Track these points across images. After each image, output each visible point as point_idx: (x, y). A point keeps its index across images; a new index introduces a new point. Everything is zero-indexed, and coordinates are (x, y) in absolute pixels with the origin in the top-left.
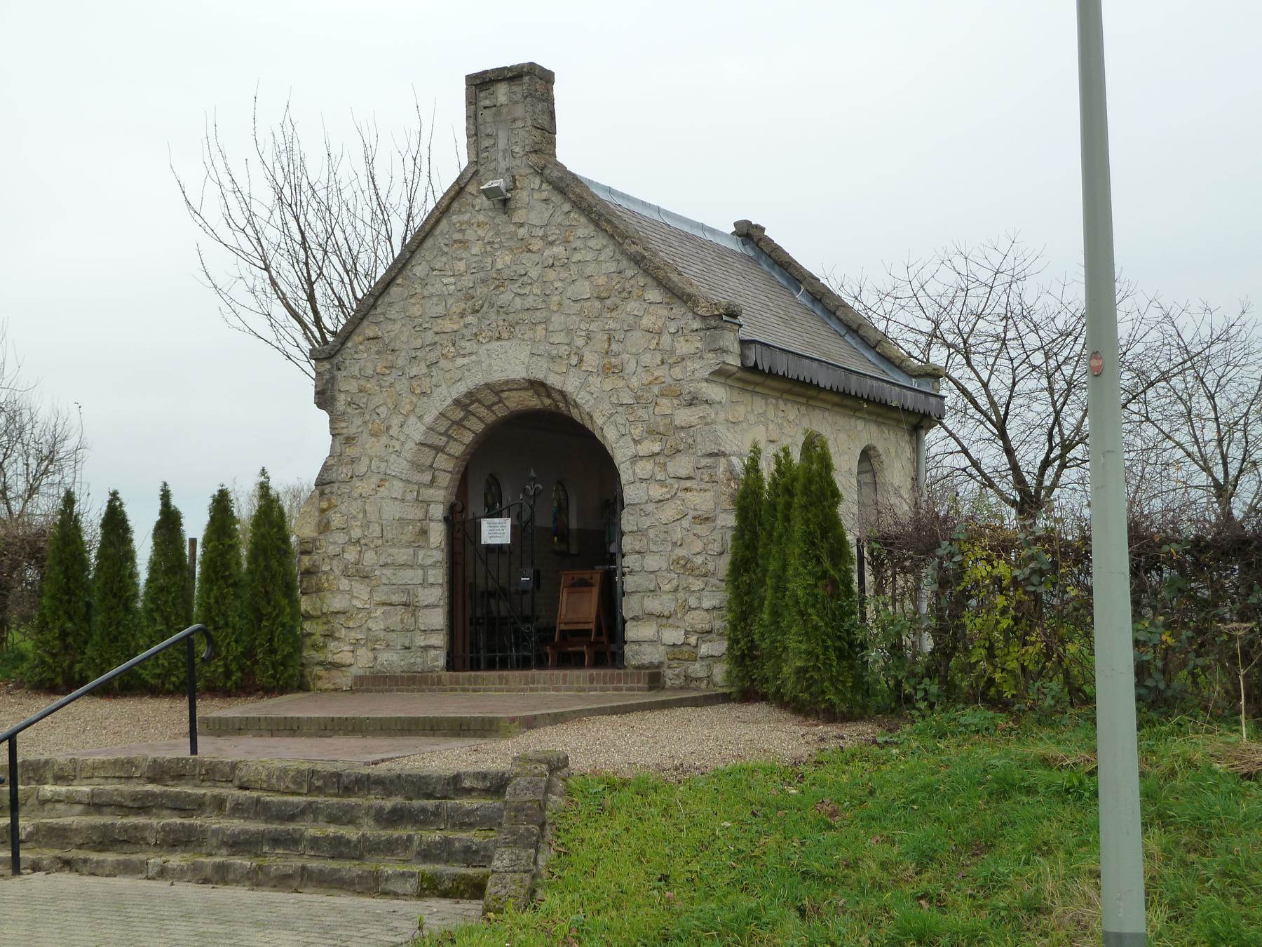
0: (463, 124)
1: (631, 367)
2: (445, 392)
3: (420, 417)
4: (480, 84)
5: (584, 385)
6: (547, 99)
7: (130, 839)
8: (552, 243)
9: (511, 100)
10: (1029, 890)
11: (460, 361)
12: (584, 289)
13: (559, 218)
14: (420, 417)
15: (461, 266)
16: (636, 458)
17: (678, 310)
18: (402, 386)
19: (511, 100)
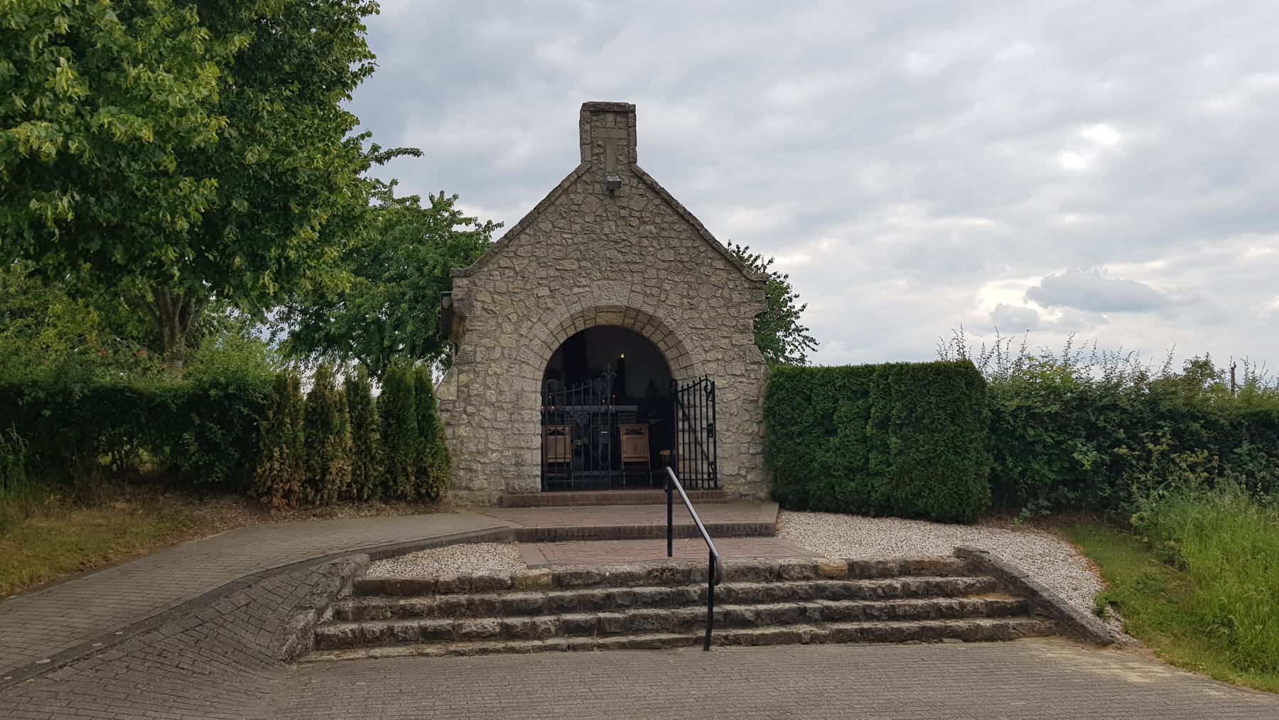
0: (662, 184)
1: (703, 306)
2: (565, 309)
3: (546, 324)
4: (593, 112)
5: (670, 314)
6: (631, 127)
7: (531, 632)
8: (646, 223)
9: (608, 124)
10: (162, 525)
11: (576, 290)
12: (669, 255)
13: (651, 207)
14: (546, 324)
15: (577, 228)
16: (706, 361)
17: (736, 275)
18: (531, 302)
19: (608, 124)
